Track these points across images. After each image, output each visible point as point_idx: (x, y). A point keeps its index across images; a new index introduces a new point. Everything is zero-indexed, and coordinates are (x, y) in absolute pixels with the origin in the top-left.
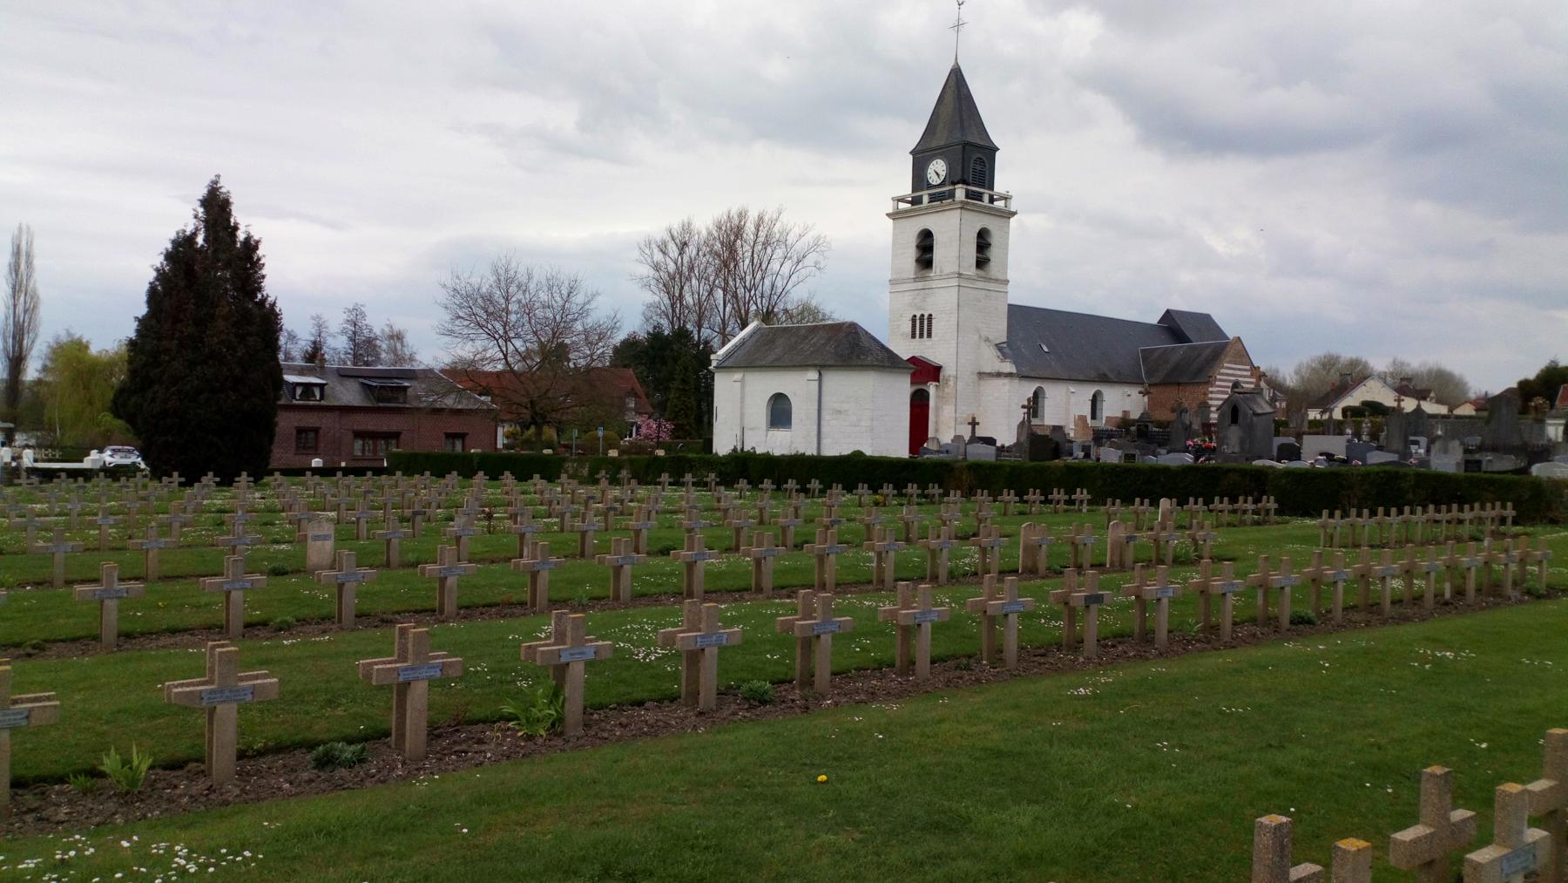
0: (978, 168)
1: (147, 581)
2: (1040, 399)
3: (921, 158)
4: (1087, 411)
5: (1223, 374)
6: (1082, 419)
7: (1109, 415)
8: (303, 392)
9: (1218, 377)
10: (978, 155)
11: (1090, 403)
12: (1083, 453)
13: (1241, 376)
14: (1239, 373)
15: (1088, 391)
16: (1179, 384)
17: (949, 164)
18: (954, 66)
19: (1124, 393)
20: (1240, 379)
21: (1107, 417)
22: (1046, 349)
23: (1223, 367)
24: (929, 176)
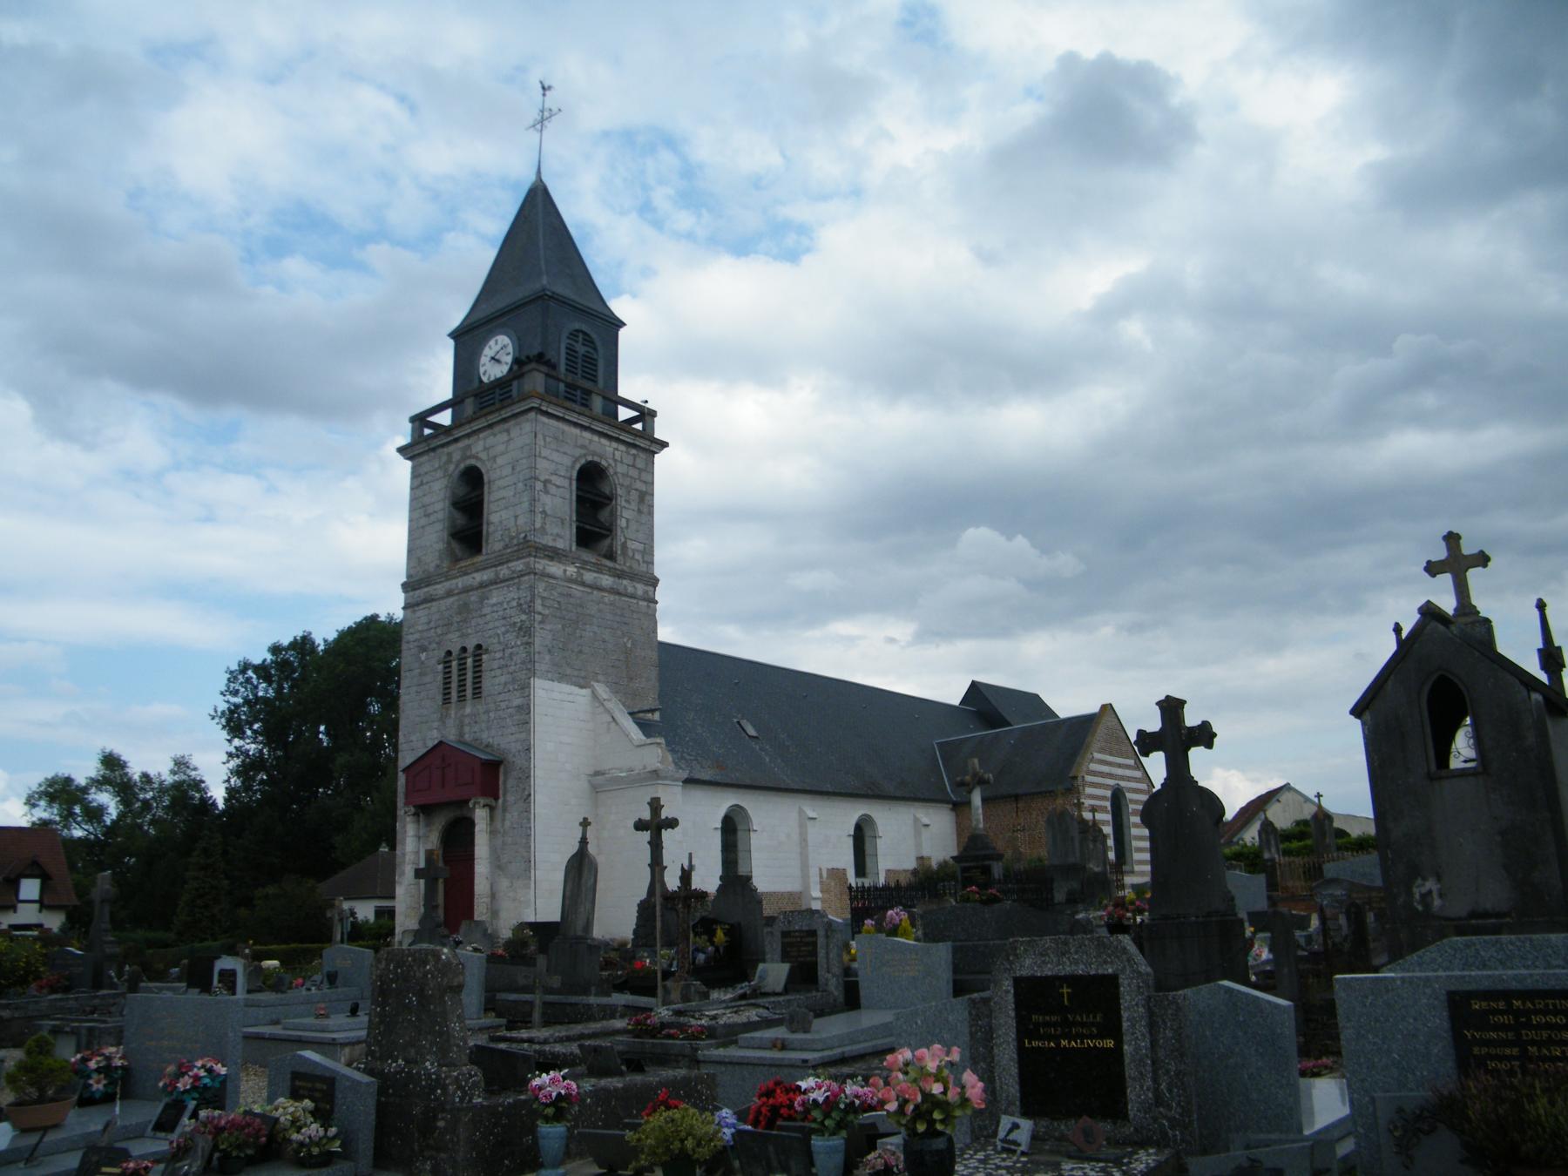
0: (581, 349)
1: (296, 1076)
2: (740, 834)
3: (468, 338)
4: (846, 861)
5: (1094, 773)
6: (837, 874)
7: (889, 867)
8: (1299, 928)
9: (1089, 778)
10: (577, 326)
11: (850, 841)
12: (786, 967)
13: (1123, 778)
14: (1120, 772)
15: (844, 816)
16: (1017, 798)
17: (519, 339)
18: (536, 181)
19: (916, 820)
20: (1123, 784)
21: (888, 871)
22: (751, 731)
23: (1092, 760)
24: (482, 370)
